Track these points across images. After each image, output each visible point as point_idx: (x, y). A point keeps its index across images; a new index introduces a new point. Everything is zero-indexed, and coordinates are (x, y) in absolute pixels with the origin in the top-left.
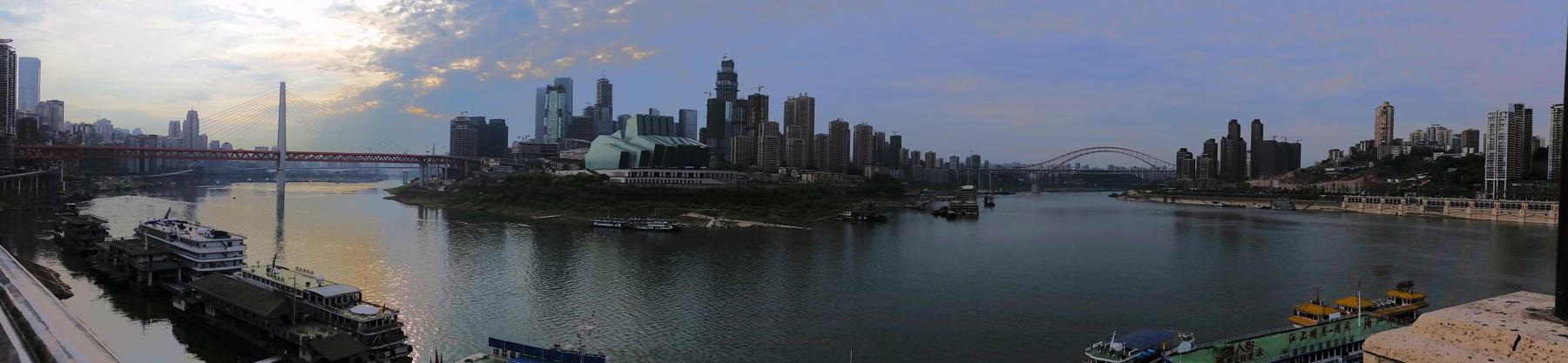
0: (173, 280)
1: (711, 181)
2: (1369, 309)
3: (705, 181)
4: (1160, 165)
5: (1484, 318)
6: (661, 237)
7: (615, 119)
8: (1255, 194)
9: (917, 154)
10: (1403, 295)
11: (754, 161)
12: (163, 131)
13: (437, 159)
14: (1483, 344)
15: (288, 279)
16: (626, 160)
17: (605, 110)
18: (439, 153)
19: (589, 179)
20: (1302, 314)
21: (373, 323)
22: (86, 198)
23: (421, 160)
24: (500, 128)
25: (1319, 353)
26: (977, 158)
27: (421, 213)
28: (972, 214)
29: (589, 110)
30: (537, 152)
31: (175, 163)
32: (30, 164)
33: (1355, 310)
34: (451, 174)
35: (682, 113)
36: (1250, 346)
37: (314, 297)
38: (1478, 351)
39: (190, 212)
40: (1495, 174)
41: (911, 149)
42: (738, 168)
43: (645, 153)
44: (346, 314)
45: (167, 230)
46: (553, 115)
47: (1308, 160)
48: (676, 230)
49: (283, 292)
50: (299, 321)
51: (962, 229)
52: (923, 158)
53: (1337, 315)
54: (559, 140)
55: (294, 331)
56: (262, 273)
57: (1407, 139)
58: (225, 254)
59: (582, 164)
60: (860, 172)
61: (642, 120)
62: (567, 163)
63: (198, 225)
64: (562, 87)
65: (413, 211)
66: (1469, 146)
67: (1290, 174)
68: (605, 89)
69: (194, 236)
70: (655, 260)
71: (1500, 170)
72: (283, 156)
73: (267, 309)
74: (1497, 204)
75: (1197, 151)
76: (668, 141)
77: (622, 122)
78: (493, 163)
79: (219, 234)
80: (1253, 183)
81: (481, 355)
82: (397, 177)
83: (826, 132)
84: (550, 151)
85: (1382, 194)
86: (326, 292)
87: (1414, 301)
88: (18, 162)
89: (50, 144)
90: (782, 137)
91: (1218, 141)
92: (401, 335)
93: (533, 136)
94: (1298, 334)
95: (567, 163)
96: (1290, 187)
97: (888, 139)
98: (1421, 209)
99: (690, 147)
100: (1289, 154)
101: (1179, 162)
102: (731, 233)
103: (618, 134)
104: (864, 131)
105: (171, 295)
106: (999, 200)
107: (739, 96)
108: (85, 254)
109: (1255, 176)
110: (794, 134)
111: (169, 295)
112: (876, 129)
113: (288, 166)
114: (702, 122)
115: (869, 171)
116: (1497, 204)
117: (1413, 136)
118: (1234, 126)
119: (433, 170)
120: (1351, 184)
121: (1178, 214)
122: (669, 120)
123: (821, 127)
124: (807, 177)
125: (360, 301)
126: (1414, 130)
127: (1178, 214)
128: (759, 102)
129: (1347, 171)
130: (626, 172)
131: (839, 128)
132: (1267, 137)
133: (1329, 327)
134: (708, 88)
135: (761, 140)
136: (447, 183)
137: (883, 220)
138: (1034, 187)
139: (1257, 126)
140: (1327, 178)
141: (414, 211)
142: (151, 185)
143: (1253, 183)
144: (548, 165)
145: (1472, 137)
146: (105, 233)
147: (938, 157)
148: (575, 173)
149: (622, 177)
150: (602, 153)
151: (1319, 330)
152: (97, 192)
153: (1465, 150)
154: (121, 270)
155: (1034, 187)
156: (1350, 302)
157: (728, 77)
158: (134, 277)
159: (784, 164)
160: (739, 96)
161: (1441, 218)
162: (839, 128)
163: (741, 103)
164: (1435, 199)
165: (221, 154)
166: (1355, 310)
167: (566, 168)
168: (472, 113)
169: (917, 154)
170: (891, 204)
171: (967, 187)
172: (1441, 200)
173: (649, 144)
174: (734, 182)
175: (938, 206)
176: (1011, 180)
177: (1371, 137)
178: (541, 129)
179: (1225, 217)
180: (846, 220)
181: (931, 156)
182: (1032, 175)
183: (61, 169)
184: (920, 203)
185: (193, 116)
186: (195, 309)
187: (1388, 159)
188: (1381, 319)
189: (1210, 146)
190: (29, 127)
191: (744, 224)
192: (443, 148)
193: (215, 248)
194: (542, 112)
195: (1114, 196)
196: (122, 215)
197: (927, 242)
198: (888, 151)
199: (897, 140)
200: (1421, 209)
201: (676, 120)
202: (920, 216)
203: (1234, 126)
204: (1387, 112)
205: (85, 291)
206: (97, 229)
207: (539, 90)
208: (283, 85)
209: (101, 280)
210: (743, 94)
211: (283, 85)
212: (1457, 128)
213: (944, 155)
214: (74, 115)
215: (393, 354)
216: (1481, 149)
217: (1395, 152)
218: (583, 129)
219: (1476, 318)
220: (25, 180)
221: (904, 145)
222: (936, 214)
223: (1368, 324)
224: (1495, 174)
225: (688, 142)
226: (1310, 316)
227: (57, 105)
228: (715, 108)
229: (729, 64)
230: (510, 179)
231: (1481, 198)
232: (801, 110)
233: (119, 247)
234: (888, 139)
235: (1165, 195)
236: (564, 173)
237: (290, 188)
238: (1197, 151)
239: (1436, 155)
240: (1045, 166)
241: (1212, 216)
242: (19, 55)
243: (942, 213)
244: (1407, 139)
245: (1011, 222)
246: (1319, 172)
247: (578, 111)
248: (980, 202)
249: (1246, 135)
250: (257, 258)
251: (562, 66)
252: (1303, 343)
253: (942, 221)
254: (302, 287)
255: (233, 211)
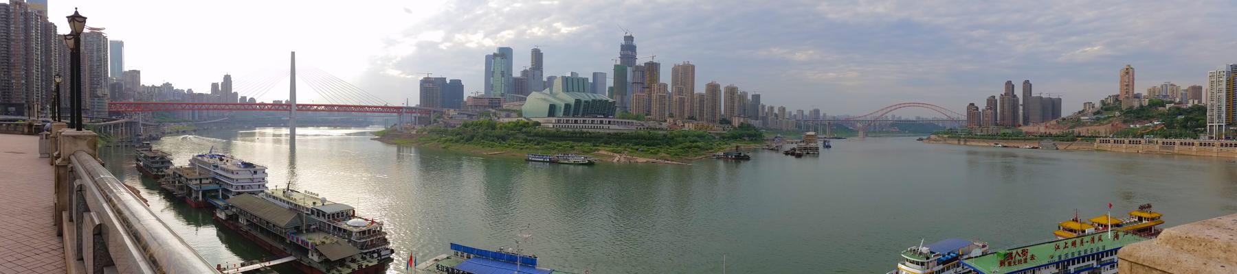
0: (216, 197)
1: (616, 127)
2: (1118, 225)
3: (612, 127)
4: (955, 116)
5: (1214, 233)
6: (580, 168)
7: (545, 79)
8: (1027, 137)
9: (772, 108)
10: (1144, 215)
11: (649, 113)
12: (207, 90)
13: (410, 110)
14: (1215, 253)
15: (298, 199)
16: (552, 110)
17: (537, 72)
18: (413, 105)
19: (526, 125)
20: (1065, 229)
21: (364, 232)
22: (157, 139)
23: (398, 110)
24: (457, 86)
25: (1078, 259)
26: (817, 111)
27: (399, 150)
28: (814, 152)
29: (525, 72)
30: (490, 103)
31: (216, 113)
32: (118, 114)
33: (1106, 226)
34: (420, 121)
35: (595, 75)
36: (1025, 252)
37: (319, 213)
38: (1211, 258)
39: (228, 147)
40: (1216, 118)
41: (767, 105)
42: (637, 118)
43: (567, 106)
44: (343, 225)
45: (211, 161)
46: (498, 75)
47: (1067, 111)
48: (591, 164)
49: (296, 209)
50: (308, 231)
51: (807, 162)
52: (776, 111)
53: (1092, 230)
54: (502, 95)
55: (304, 237)
56: (280, 195)
57: (1145, 93)
58: (252, 180)
59: (520, 115)
60: (729, 123)
61: (565, 80)
62: (509, 113)
63: (232, 158)
64: (504, 54)
65: (393, 149)
66: (1194, 98)
67: (1053, 122)
68: (537, 56)
69: (229, 166)
70: (577, 191)
71: (1219, 117)
72: (294, 108)
73: (284, 220)
74: (1127, 141)
75: (982, 105)
76: (585, 97)
77: (551, 79)
78: (452, 112)
79: (247, 165)
80: (1024, 129)
81: (445, 256)
82: (379, 124)
83: (703, 91)
84: (495, 103)
85: (1126, 136)
86: (328, 211)
87: (1153, 219)
88: (111, 113)
89: (132, 101)
90: (670, 96)
91: (998, 98)
92: (385, 241)
93: (482, 91)
94: (1062, 244)
95: (509, 113)
96: (1054, 132)
97: (750, 97)
98: (1157, 147)
99: (600, 101)
100: (1051, 108)
101: (969, 113)
102: (631, 168)
103: (547, 91)
104: (732, 91)
105: (214, 208)
106: (833, 143)
107: (638, 63)
108: (157, 177)
109: (1026, 122)
110: (680, 92)
111: (214, 208)
112: (741, 89)
113: (299, 115)
114: (610, 82)
115: (736, 122)
116: (1216, 142)
117: (1150, 91)
118: (1010, 86)
119: (407, 118)
120: (1102, 130)
121: (969, 153)
122: (585, 80)
123: (700, 88)
124: (690, 127)
125: (353, 216)
126: (1150, 86)
127: (969, 153)
128: (653, 68)
129: (1098, 119)
130: (553, 119)
131: (713, 89)
132: (1035, 93)
133: (1085, 239)
134: (615, 58)
135: (654, 96)
136: (418, 127)
137: (747, 158)
138: (861, 133)
139: (1027, 86)
140: (1084, 124)
141: (394, 149)
142: (200, 129)
143: (1024, 129)
144: (495, 114)
145: (1196, 91)
146: (169, 162)
147: (787, 110)
148: (515, 120)
149: (550, 124)
150: (534, 105)
151: (1078, 241)
152: (164, 134)
153: (1191, 102)
154: (181, 188)
155: (861, 133)
156: (1103, 221)
157: (629, 48)
158: (190, 194)
159: (671, 116)
160: (638, 63)
161: (1173, 154)
162: (713, 89)
163: (638, 68)
164: (1169, 140)
165: (250, 105)
166: (1106, 226)
167: (508, 116)
168: (435, 75)
169: (772, 108)
170: (753, 146)
171: (809, 136)
172: (1173, 140)
173: (570, 99)
174: (634, 128)
175: (788, 147)
176: (842, 128)
177: (1117, 92)
178: (489, 86)
179: (1004, 155)
180: (719, 158)
181: (783, 109)
182: (859, 125)
183: (139, 118)
184: (774, 145)
185: (227, 79)
186: (233, 218)
187: (1130, 111)
188: (1127, 233)
189: (992, 102)
190: (115, 88)
191: (641, 160)
192: (414, 101)
193: (245, 175)
194: (489, 73)
195: (920, 140)
196: (182, 152)
197: (773, 171)
198: (752, 106)
199: (757, 98)
200: (1157, 147)
201: (591, 81)
202: (774, 154)
203: (1010, 86)
204: (1128, 72)
205: (157, 202)
206: (165, 161)
207: (488, 57)
208: (293, 54)
209: (169, 196)
210: (641, 60)
211: (293, 54)
212: (1184, 84)
213: (792, 109)
214: (146, 81)
215: (380, 255)
216: (1204, 101)
217: (1136, 104)
218: (521, 87)
219: (1208, 232)
220: (116, 126)
221: (762, 102)
222: (787, 153)
223: (1117, 236)
224: (1216, 118)
225: (599, 97)
226: (1071, 230)
227: (135, 74)
228: (620, 72)
229: (629, 39)
230: (466, 126)
231: (1204, 138)
232: (685, 73)
233: (178, 174)
234: (750, 97)
235: (959, 139)
236: (507, 120)
237: (299, 131)
238: (982, 105)
239: (1168, 106)
240: (869, 118)
241: (994, 155)
242: (110, 38)
243: (792, 153)
244: (1145, 93)
245: (842, 156)
246: (1076, 121)
247: (517, 73)
248: (820, 144)
249: (1019, 92)
250: (276, 181)
251: (506, 38)
252: (1066, 251)
253: (791, 158)
254: (310, 205)
255: (262, 149)
